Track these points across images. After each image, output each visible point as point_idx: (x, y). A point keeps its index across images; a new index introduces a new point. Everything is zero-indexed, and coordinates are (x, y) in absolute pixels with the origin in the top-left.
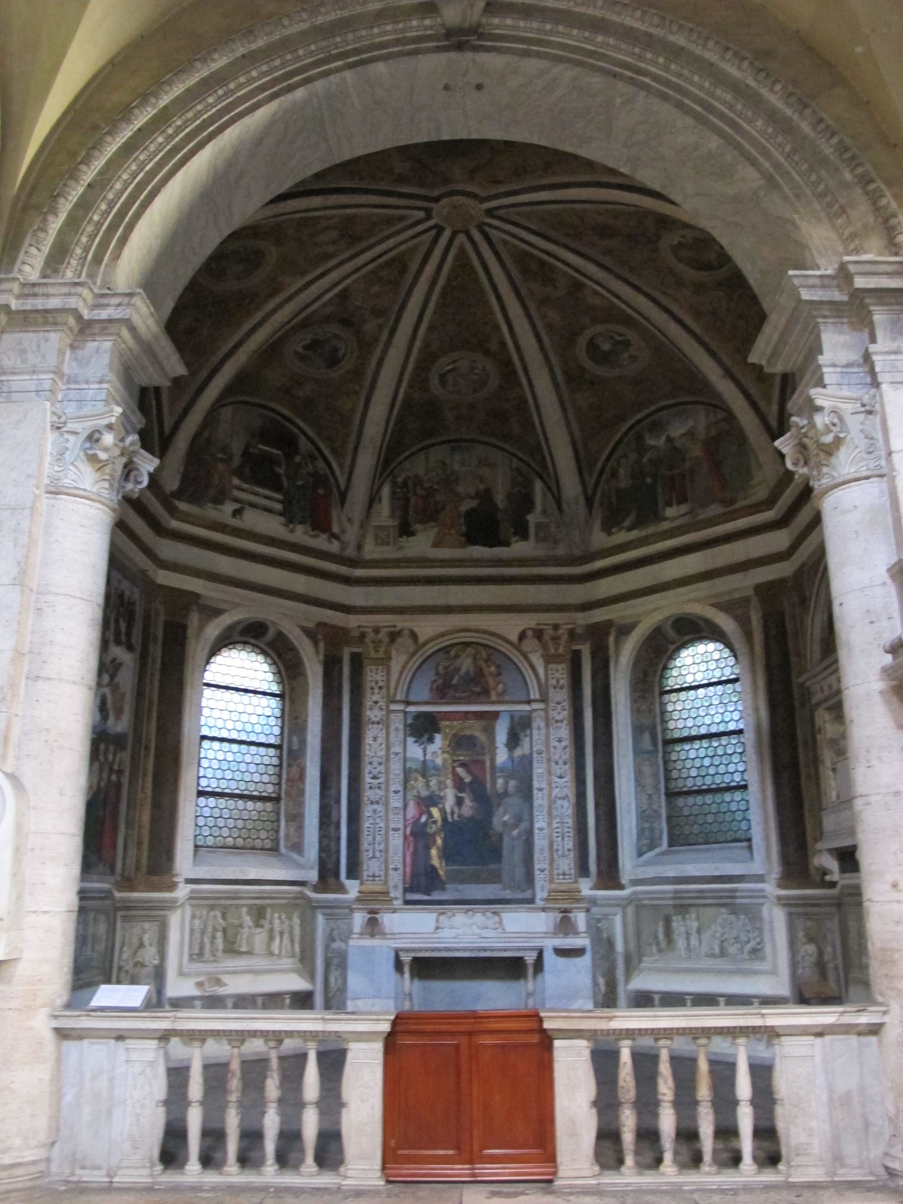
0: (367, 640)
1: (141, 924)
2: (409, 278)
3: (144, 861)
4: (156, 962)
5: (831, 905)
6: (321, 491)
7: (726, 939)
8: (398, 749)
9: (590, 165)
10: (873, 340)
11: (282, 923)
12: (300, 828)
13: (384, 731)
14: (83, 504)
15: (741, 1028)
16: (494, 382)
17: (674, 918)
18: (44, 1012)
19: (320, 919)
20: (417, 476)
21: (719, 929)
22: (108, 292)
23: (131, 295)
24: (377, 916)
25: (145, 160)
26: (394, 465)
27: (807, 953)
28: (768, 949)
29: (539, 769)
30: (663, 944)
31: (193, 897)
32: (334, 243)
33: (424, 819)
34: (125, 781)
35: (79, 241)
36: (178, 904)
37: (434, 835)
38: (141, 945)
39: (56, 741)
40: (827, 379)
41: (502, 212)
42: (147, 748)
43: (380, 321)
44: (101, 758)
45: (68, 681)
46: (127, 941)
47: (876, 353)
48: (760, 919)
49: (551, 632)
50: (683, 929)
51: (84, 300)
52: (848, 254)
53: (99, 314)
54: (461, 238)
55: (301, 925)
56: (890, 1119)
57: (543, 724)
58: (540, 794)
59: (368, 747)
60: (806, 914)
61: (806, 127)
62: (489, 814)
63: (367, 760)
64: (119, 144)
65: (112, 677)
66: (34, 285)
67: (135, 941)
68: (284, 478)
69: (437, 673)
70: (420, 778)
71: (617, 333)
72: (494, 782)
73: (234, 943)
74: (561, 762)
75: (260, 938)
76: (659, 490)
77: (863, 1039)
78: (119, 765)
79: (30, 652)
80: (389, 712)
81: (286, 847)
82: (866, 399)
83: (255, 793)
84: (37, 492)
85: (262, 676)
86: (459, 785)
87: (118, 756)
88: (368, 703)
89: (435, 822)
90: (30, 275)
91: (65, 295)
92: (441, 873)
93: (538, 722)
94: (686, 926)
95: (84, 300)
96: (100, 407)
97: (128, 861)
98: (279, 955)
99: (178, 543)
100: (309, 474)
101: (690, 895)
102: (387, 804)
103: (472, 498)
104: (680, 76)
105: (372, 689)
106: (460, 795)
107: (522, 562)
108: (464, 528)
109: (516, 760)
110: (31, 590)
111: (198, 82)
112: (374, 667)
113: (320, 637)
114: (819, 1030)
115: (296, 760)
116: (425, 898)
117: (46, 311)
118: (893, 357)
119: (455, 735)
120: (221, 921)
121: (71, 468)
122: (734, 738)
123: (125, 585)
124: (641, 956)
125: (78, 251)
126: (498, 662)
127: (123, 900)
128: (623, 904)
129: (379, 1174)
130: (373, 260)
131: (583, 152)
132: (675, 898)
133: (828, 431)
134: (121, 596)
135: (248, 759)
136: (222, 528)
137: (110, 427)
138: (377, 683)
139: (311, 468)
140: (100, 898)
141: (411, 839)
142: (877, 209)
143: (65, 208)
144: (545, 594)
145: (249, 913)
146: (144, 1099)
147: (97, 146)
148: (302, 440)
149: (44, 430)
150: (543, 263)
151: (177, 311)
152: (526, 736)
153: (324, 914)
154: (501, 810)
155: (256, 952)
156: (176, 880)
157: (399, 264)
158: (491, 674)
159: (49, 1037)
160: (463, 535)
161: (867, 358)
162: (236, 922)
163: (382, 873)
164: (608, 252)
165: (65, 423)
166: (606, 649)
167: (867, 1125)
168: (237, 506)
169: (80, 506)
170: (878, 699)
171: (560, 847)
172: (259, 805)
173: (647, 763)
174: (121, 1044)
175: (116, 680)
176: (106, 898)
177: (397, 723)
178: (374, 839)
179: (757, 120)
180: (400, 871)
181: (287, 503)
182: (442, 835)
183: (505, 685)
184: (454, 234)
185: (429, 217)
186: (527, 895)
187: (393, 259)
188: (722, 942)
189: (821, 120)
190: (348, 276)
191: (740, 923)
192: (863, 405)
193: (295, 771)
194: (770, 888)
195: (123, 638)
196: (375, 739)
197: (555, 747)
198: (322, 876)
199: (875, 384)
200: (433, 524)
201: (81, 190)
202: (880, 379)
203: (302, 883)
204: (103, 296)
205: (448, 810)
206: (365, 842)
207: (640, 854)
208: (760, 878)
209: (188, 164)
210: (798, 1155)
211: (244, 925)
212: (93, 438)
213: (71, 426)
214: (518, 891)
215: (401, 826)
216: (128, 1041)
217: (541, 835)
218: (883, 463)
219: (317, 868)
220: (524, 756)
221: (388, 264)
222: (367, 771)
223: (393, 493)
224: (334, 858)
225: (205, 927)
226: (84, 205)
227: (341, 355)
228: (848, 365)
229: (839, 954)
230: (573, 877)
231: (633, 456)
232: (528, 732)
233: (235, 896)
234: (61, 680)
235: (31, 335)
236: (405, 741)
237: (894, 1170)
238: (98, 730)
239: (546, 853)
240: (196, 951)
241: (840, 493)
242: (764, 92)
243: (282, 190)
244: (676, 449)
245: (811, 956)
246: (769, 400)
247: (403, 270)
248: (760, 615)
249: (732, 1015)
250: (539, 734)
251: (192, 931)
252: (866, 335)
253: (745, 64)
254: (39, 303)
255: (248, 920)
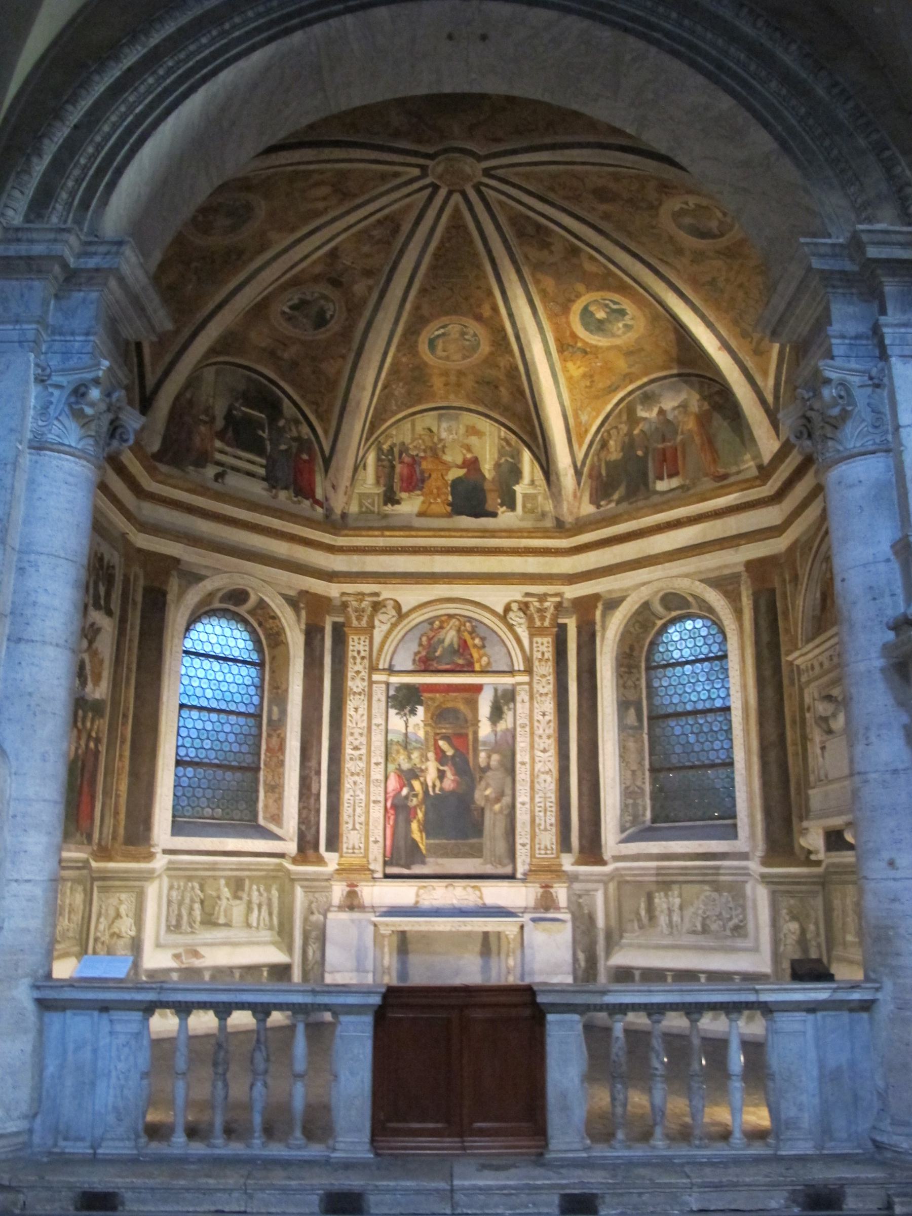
0: (350, 609)
1: (118, 895)
2: (401, 239)
3: (121, 831)
4: (133, 933)
5: (814, 883)
6: (305, 457)
7: (708, 917)
8: (378, 720)
9: (592, 125)
10: (883, 311)
11: (261, 894)
12: (279, 800)
13: (366, 702)
14: (67, 460)
15: (734, 1003)
16: (485, 348)
17: (657, 894)
18: (26, 982)
19: (299, 892)
20: (403, 444)
21: (701, 906)
22: (96, 239)
23: (120, 243)
24: (356, 889)
25: (134, 102)
26: (379, 432)
27: (790, 930)
28: (751, 926)
29: (522, 744)
30: (877, 985)
31: (171, 868)
32: (325, 199)
33: (405, 791)
34: (103, 748)
35: (65, 184)
36: (155, 875)
37: (415, 808)
38: (118, 916)
39: (38, 705)
40: (836, 352)
41: (500, 172)
42: (125, 716)
43: (371, 282)
44: (79, 724)
45: (51, 644)
46: (103, 911)
47: (887, 325)
48: (744, 896)
49: (537, 604)
50: (665, 906)
51: (71, 248)
52: (860, 223)
53: (86, 263)
54: (457, 198)
55: (279, 897)
56: (879, 1093)
57: (527, 698)
58: (523, 768)
59: (348, 718)
60: (788, 892)
61: (820, 91)
62: (471, 789)
63: (347, 731)
64: (108, 84)
65: (91, 643)
66: (17, 230)
67: (112, 913)
68: (268, 443)
69: (420, 645)
70: (402, 751)
71: (611, 301)
72: (476, 755)
73: (212, 914)
74: (544, 737)
75: (238, 910)
76: (650, 465)
77: (856, 1015)
78: (97, 733)
79: (11, 613)
80: (371, 683)
81: (265, 818)
82: (874, 372)
83: (234, 763)
84: (20, 447)
85: (241, 644)
86: (441, 757)
87: (97, 722)
88: (350, 674)
89: (416, 796)
90: (13, 219)
91: (49, 241)
92: (422, 847)
93: (522, 695)
94: (669, 903)
95: (71, 248)
96: (87, 360)
97: (105, 830)
98: (257, 928)
99: (158, 507)
100: (295, 439)
101: (671, 871)
102: (368, 776)
103: (461, 467)
104: (693, 32)
105: (354, 658)
106: (441, 768)
107: (510, 533)
108: (450, 498)
109: (499, 734)
110: (13, 549)
111: (192, 21)
112: (356, 638)
113: (302, 605)
114: (812, 1006)
115: (275, 730)
116: (405, 871)
117: (30, 258)
118: (903, 330)
119: (438, 707)
120: (199, 892)
121: (56, 422)
122: (720, 716)
123: (105, 549)
124: (622, 932)
125: (64, 195)
126: (482, 635)
127: (100, 871)
128: (605, 880)
129: (367, 1147)
130: (366, 218)
131: (586, 110)
132: (658, 875)
133: (836, 405)
134: (101, 559)
135: (227, 728)
136: (202, 490)
137: (96, 382)
138: (359, 652)
139: (294, 433)
140: (78, 868)
141: (392, 812)
142: (890, 177)
143: (50, 149)
144: (532, 565)
145: (227, 885)
146: (129, 1071)
147: (85, 84)
148: (286, 402)
149: (27, 382)
150: (539, 227)
151: (163, 267)
152: (509, 709)
153: (302, 887)
154: (483, 783)
155: (234, 923)
156: (153, 850)
157: (392, 224)
158: (475, 646)
159: (30, 1007)
160: (449, 505)
161: (876, 332)
162: (214, 894)
163: (362, 846)
164: (606, 216)
165: (49, 376)
166: (593, 623)
167: (856, 1098)
168: (219, 469)
169: (65, 463)
170: (878, 676)
171: (543, 822)
172: (238, 775)
173: (632, 739)
174: (105, 1016)
175: (95, 645)
176: (83, 868)
177: (379, 693)
178: (354, 810)
179: (771, 81)
180: (381, 844)
181: (270, 467)
182: (423, 809)
183: (489, 658)
184: (450, 193)
185: (424, 174)
186: (508, 870)
187: (386, 218)
188: (704, 919)
189: (835, 84)
190: (338, 234)
191: (724, 900)
192: (871, 378)
193: (275, 741)
194: (754, 866)
195: (102, 602)
196: (356, 709)
197: (538, 721)
198: (301, 848)
199: (884, 356)
200: (418, 492)
201: (66, 131)
202: (889, 352)
203: (282, 856)
204: (90, 243)
205: (430, 784)
206: (346, 811)
207: (623, 830)
208: (744, 856)
209: (181, 108)
210: (788, 1129)
211: (222, 897)
212: (79, 392)
213: (55, 379)
214: (499, 866)
215: (382, 799)
216: (112, 1012)
217: (524, 809)
218: (890, 437)
219: (296, 839)
220: (507, 729)
221: (379, 222)
222: (347, 742)
223: (379, 459)
224: (313, 830)
225: (183, 897)
226: (70, 148)
227: (328, 316)
228: (858, 337)
229: (822, 931)
230: (554, 852)
231: (624, 428)
232: (512, 705)
233: (213, 867)
234: (44, 643)
235: (14, 283)
236: (387, 712)
237: (882, 1143)
238: (77, 696)
239: (528, 829)
240: (174, 922)
241: (844, 467)
242: (779, 52)
243: (273, 142)
244: (668, 422)
245: (793, 933)
246: (765, 374)
247: (396, 230)
248: (750, 592)
249: (728, 990)
250: (523, 708)
251: (169, 902)
252: (876, 306)
253: (760, 23)
254: (23, 249)
255: (226, 892)
